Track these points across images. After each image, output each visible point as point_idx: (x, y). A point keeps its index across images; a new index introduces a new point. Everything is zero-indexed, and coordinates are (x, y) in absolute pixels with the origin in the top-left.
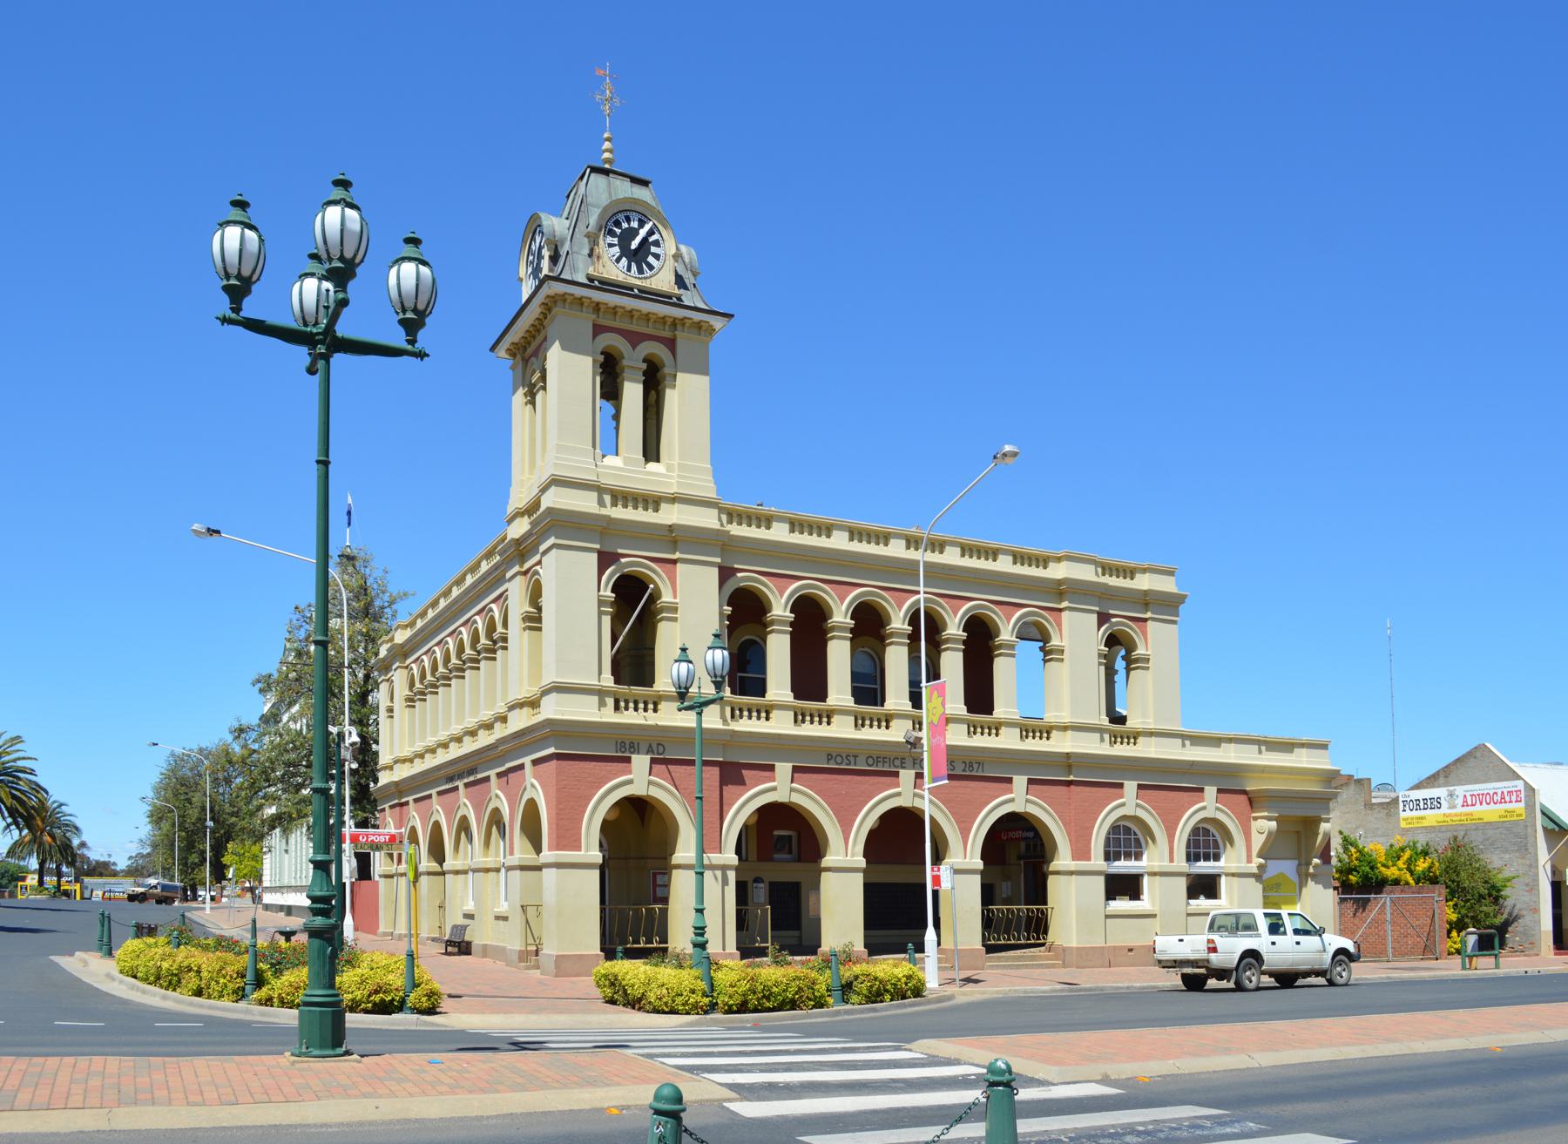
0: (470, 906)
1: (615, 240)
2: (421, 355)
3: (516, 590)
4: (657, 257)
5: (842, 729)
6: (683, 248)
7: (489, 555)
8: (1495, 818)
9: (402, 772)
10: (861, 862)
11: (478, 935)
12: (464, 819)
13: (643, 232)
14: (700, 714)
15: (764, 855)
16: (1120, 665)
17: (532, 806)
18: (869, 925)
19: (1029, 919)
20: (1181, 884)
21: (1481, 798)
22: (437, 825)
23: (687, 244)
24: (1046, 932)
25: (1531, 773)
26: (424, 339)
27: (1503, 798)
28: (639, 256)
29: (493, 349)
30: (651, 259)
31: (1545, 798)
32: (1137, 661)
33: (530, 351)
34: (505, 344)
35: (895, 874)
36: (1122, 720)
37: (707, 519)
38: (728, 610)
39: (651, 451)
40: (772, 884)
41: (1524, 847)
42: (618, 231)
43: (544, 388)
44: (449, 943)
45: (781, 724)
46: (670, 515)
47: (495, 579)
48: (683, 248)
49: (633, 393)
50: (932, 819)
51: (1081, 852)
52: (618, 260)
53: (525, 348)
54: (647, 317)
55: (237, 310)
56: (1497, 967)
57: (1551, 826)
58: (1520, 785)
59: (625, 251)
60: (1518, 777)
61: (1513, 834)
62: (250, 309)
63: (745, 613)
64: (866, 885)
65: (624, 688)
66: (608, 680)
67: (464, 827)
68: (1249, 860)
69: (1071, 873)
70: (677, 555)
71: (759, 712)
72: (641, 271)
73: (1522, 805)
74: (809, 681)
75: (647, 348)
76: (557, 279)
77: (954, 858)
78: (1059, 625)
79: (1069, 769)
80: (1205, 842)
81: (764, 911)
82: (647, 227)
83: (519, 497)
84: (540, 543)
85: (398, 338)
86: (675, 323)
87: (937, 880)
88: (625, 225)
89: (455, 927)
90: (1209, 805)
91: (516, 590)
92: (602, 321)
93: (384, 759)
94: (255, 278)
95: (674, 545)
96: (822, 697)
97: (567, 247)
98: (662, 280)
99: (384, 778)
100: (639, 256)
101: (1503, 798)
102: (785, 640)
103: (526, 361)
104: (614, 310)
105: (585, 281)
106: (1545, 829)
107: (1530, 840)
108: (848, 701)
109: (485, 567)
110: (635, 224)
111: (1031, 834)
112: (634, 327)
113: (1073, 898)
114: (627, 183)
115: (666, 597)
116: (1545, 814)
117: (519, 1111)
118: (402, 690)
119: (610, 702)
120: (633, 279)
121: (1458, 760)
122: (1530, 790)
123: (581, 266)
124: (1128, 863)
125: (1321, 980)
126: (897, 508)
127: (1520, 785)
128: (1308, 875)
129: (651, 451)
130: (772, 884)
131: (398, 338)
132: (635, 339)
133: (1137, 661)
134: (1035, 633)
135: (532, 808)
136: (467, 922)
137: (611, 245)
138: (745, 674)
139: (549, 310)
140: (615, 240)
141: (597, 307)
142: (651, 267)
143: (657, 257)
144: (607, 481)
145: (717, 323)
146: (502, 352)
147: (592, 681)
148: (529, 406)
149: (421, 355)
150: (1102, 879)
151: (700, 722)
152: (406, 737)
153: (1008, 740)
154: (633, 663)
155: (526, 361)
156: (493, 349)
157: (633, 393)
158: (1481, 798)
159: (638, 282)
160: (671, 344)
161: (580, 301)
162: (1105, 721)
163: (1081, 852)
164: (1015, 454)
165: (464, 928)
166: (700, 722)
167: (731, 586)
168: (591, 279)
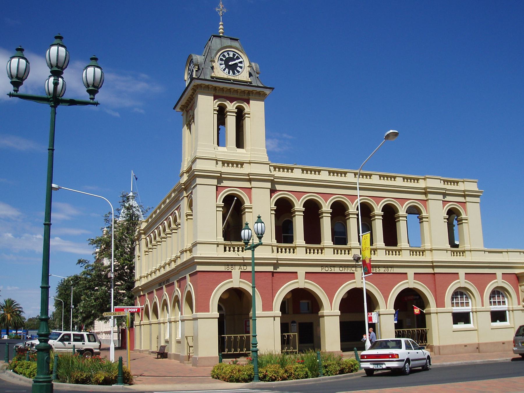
0: (167, 337)
1: (223, 62)
2: (97, 104)
3: (184, 203)
4: (241, 67)
5: (328, 255)
6: (253, 64)
7: (174, 191)
9: (144, 281)
10: (339, 313)
11: (173, 350)
12: (165, 300)
14: (253, 251)
15: (297, 310)
16: (455, 223)
17: (189, 293)
18: (342, 340)
19: (418, 334)
20: (489, 316)
22: (155, 303)
23: (254, 62)
24: (426, 339)
26: (98, 97)
28: (233, 68)
29: (174, 108)
30: (238, 69)
33: (189, 108)
34: (179, 106)
35: (352, 317)
36: (457, 246)
37: (264, 170)
39: (240, 143)
40: (299, 324)
42: (224, 59)
43: (194, 122)
44: (159, 353)
45: (300, 254)
46: (247, 169)
47: (176, 201)
48: (253, 64)
49: (231, 121)
50: (369, 293)
52: (224, 70)
53: (187, 107)
54: (236, 91)
55: (16, 91)
59: (227, 66)
62: (22, 90)
63: (283, 209)
64: (341, 323)
65: (228, 243)
66: (221, 239)
67: (165, 304)
68: (519, 304)
72: (234, 73)
74: (313, 236)
76: (198, 79)
77: (382, 309)
78: (425, 207)
81: (294, 334)
83: (185, 167)
84: (191, 185)
85: (85, 96)
87: (370, 319)
88: (227, 56)
89: (162, 346)
91: (184, 203)
92: (217, 94)
93: (137, 277)
94: (24, 78)
96: (319, 242)
97: (203, 66)
98: (243, 75)
99: (137, 284)
100: (233, 68)
103: (187, 112)
104: (222, 89)
105: (210, 79)
108: (303, 243)
109: (173, 195)
111: (418, 297)
112: (232, 96)
114: (229, 41)
115: (247, 204)
118: (144, 248)
119: (275, 249)
120: (231, 76)
123: (208, 73)
124: (457, 308)
129: (240, 143)
130: (299, 324)
131: (85, 96)
134: (414, 211)
135: (189, 294)
136: (166, 344)
137: (221, 64)
138: (284, 234)
139: (195, 91)
140: (223, 62)
141: (215, 88)
142: (238, 72)
143: (241, 67)
144: (219, 157)
145: (267, 92)
146: (178, 109)
147: (214, 240)
148: (9, 93)
149: (97, 104)
150: (489, 313)
151: (253, 255)
152: (147, 266)
153: (405, 256)
155: (187, 112)
156: (174, 108)
157: (231, 121)
159: (233, 78)
161: (208, 87)
162: (448, 246)
163: (440, 303)
164: (396, 134)
165: (164, 347)
166: (253, 255)
167: (277, 196)
168: (212, 77)
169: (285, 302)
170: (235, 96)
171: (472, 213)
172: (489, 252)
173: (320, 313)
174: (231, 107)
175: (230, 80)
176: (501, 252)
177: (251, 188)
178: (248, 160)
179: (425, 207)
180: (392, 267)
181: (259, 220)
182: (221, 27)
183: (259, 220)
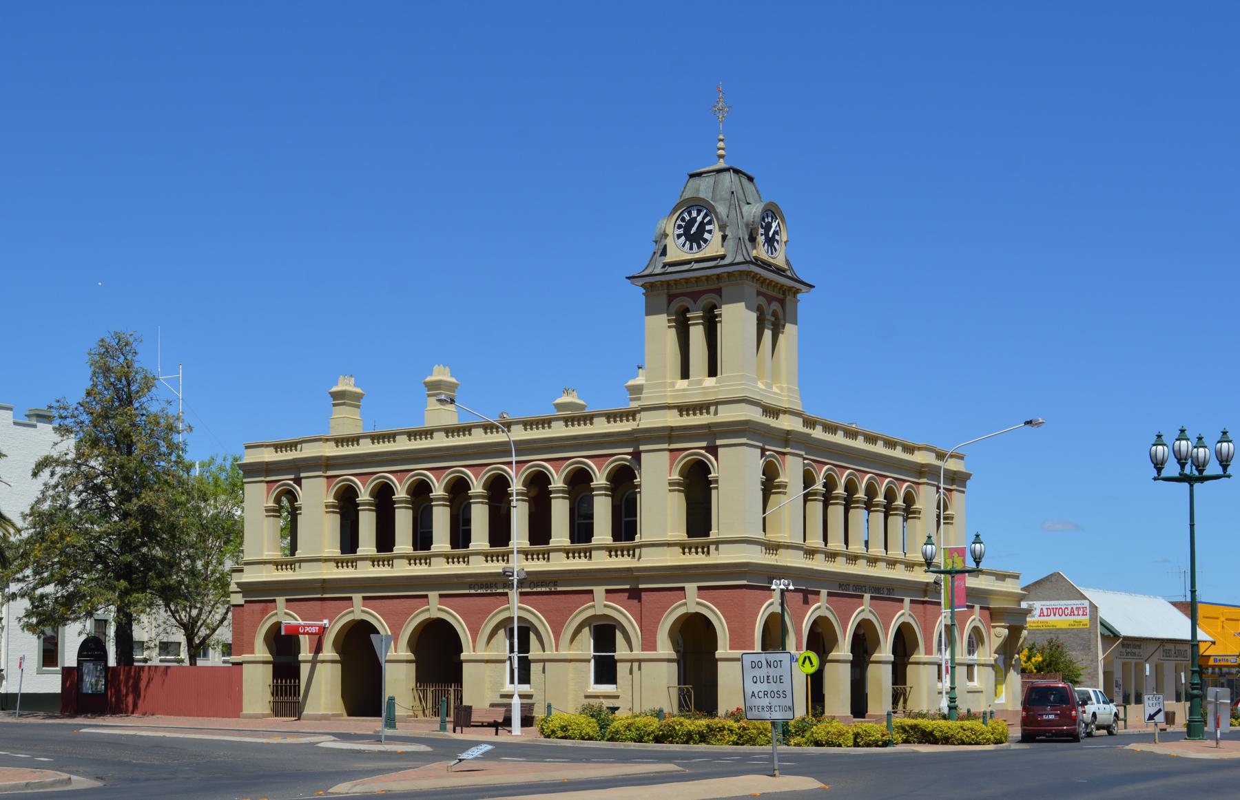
8: (1065, 626)
13: (699, 219)
21: (1054, 611)
25: (1092, 595)
27: (1072, 611)
31: (1105, 614)
32: (914, 512)
38: (637, 481)
41: (1088, 648)
49: (697, 334)
51: (649, 644)
56: (1194, 730)
57: (1107, 633)
58: (1086, 603)
60: (1085, 598)
61: (1080, 636)
69: (925, 663)
70: (788, 450)
71: (697, 549)
72: (699, 247)
73: (1087, 617)
75: (704, 300)
79: (555, 584)
82: (702, 214)
86: (719, 277)
95: (786, 443)
98: (779, 260)
101: (1072, 611)
106: (1102, 635)
107: (1093, 642)
110: (694, 214)
112: (770, 292)
113: (486, 678)
116: (1104, 624)
117: (758, 793)
121: (1037, 583)
122: (1094, 608)
125: (1104, 732)
126: (885, 412)
127: (1086, 603)
128: (1010, 665)
132: (695, 296)
133: (914, 512)
138: (349, 541)
141: (668, 283)
142: (706, 241)
154: (699, 520)
157: (697, 334)
158: (1054, 611)
160: (718, 292)
175: (770, 265)
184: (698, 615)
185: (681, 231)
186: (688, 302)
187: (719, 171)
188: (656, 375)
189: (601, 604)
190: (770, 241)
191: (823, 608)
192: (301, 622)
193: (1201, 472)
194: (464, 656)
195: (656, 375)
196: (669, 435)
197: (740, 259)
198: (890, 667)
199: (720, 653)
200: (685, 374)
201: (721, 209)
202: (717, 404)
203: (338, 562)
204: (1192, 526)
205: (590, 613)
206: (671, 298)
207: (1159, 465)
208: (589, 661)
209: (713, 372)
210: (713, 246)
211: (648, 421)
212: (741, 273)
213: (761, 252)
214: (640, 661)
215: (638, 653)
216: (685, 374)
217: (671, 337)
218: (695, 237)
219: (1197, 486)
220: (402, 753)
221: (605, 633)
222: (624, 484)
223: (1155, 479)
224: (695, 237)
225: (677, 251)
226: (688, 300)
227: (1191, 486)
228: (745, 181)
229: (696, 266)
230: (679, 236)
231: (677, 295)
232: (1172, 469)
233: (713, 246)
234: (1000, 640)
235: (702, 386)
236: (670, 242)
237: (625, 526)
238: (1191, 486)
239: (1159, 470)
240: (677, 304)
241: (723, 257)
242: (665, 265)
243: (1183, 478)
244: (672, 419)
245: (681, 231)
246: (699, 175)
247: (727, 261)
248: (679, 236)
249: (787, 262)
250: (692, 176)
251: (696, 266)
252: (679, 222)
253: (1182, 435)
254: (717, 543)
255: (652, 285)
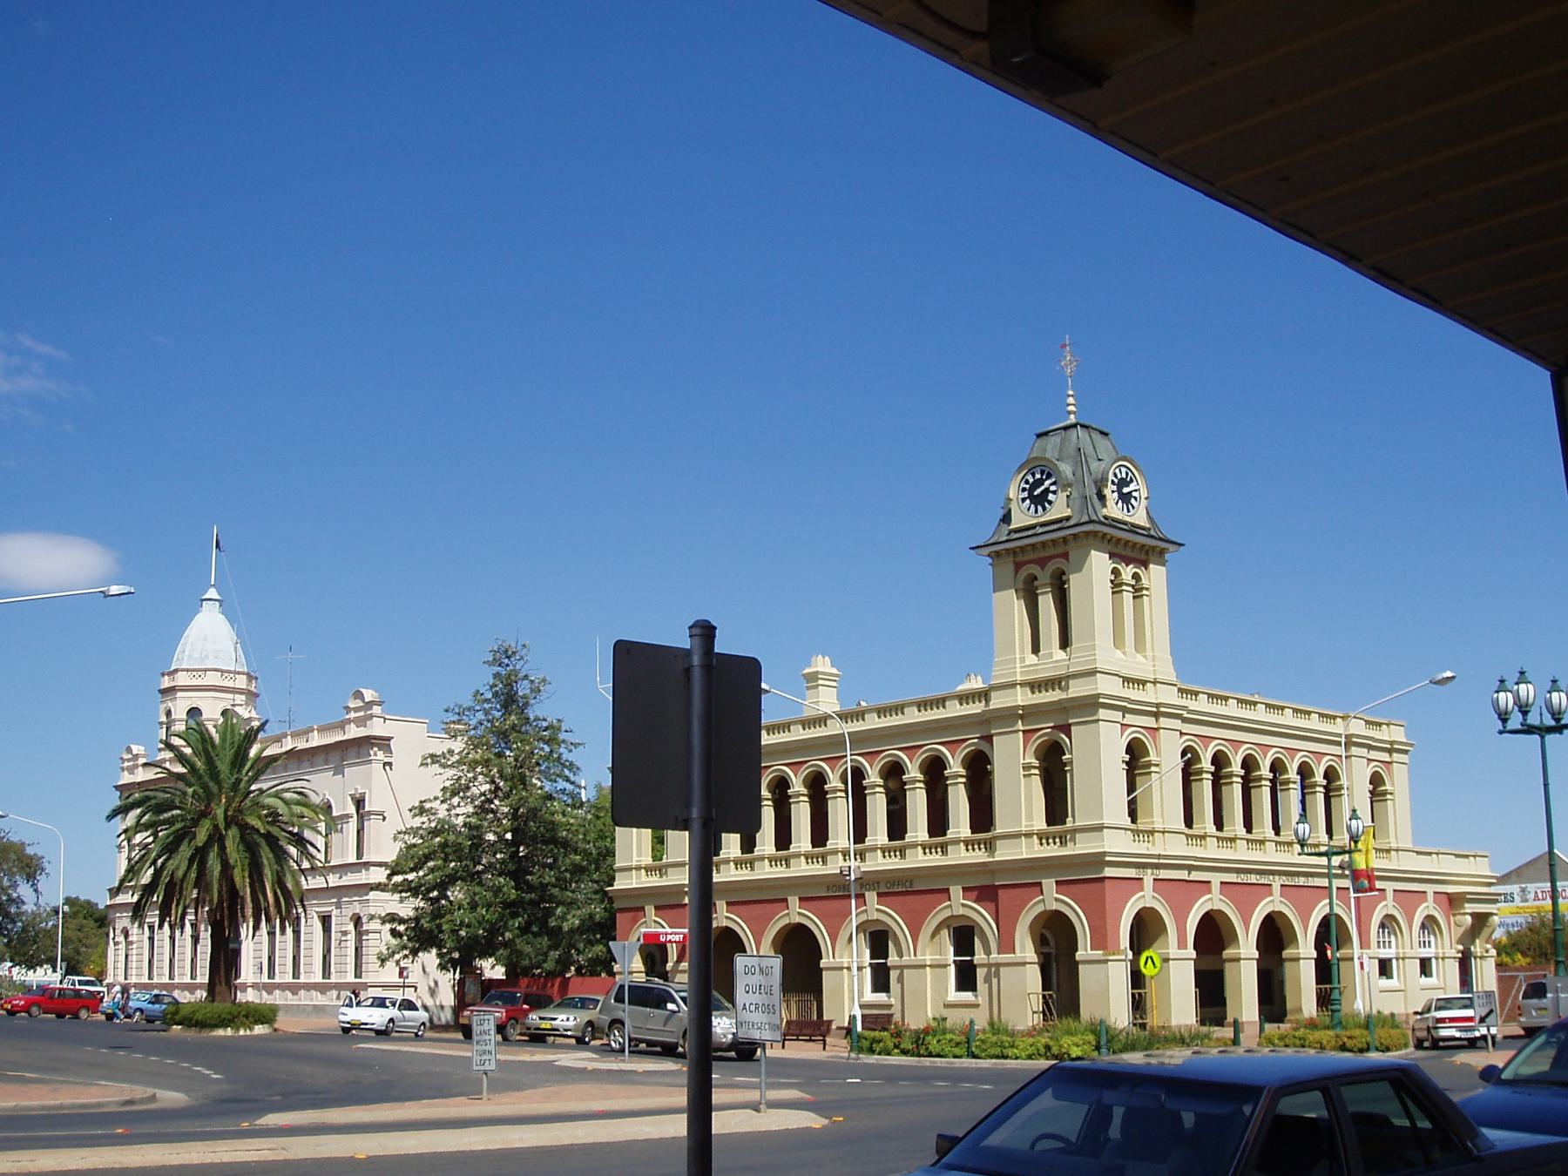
35: (1209, 964)
49: (1047, 603)
51: (1007, 945)
72: (1044, 509)
75: (1051, 567)
78: (1154, 739)
80: (879, 941)
86: (1065, 540)
90: (874, 908)
92: (1020, 558)
98: (1139, 517)
99: (621, 883)
102: (962, 789)
141: (1013, 552)
142: (1050, 503)
157: (1047, 603)
160: (1065, 556)
168: (1106, 518)
169: (1042, 935)
170: (1134, 555)
171: (1399, 782)
172: (1457, 856)
173: (1287, 953)
174: (1127, 572)
175: (1125, 523)
176: (1430, 854)
177: (1157, 729)
178: (1151, 677)
179: (1154, 739)
180: (1298, 874)
181: (1354, 815)
182: (1071, 400)
183: (1354, 815)
184: (1058, 913)
185: (1026, 494)
186: (1034, 569)
187: (1066, 428)
188: (1013, 652)
189: (959, 904)
190: (1126, 498)
191: (1277, 903)
192: (669, 930)
193: (1558, 720)
194: (823, 963)
195: (1013, 652)
196: (1029, 713)
197: (1085, 518)
198: (1037, 969)
199: (1080, 955)
200: (1036, 649)
201: (1066, 469)
202: (1069, 677)
203: (1043, 837)
204: (1546, 785)
205: (947, 913)
206: (1018, 566)
207: (1503, 717)
208: (946, 966)
209: (1065, 643)
210: (1059, 508)
211: (999, 701)
212: (1087, 533)
213: (1114, 509)
214: (998, 965)
215: (995, 957)
216: (1036, 649)
217: (1019, 607)
218: (1040, 500)
219: (1549, 738)
220: (595, 1070)
221: (964, 937)
222: (979, 770)
223: (1501, 732)
224: (1040, 500)
225: (1023, 516)
226: (1038, 566)
227: (1542, 738)
228: (1097, 437)
229: (1041, 530)
230: (1024, 500)
231: (1025, 563)
232: (1515, 721)
233: (1059, 508)
234: (1462, 930)
235: (1055, 658)
236: (1014, 506)
237: (982, 817)
238: (1542, 738)
239: (1504, 721)
240: (1023, 573)
241: (1068, 519)
242: (1010, 532)
243: (1529, 730)
244: (1022, 698)
245: (1026, 494)
246: (1046, 434)
247: (1072, 522)
248: (1024, 500)
249: (1150, 519)
250: (1039, 436)
251: (1041, 530)
252: (1023, 485)
253: (1522, 677)
254: (1075, 831)
255: (998, 554)
